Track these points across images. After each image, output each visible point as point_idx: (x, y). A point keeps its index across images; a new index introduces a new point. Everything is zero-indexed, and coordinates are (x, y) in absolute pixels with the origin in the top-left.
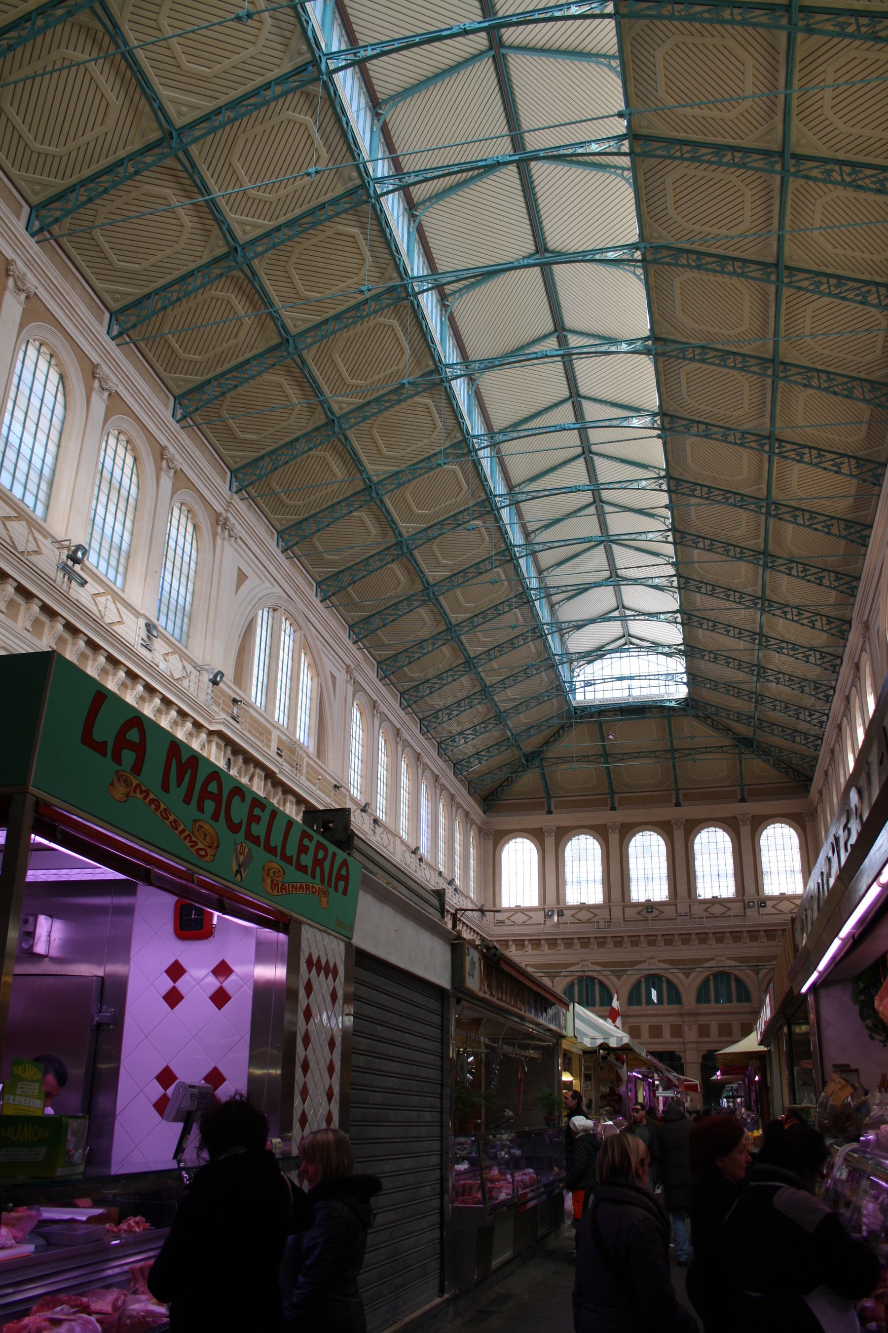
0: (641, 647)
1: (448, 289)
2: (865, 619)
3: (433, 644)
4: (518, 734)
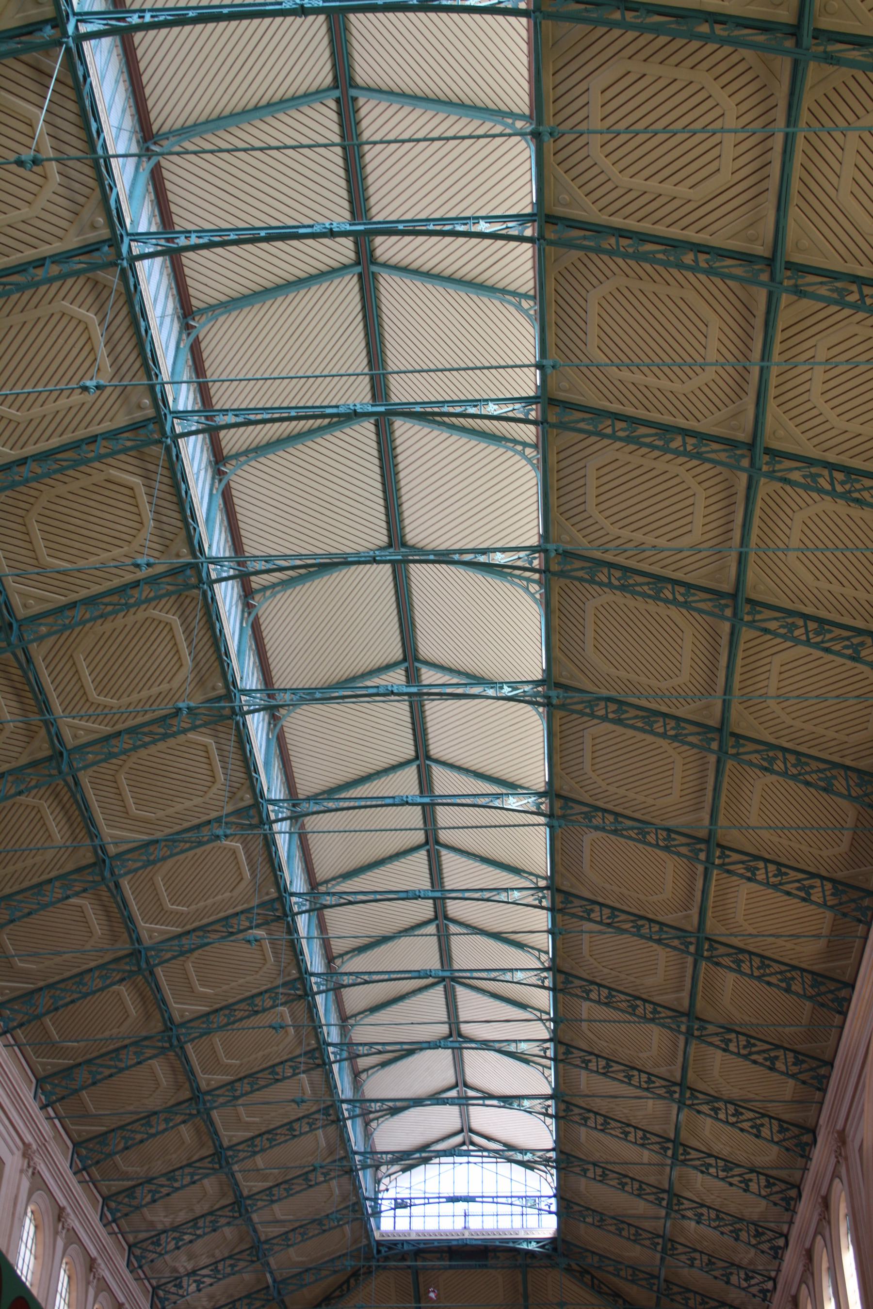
0: (486, 1150)
1: (257, 581)
2: (839, 1126)
3: (167, 1120)
4: (283, 1281)
